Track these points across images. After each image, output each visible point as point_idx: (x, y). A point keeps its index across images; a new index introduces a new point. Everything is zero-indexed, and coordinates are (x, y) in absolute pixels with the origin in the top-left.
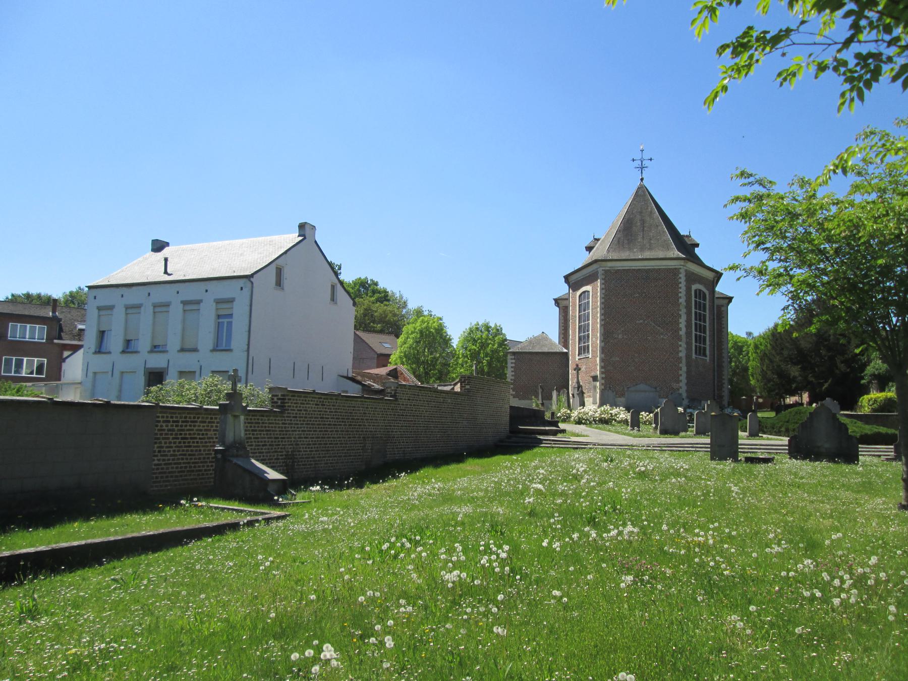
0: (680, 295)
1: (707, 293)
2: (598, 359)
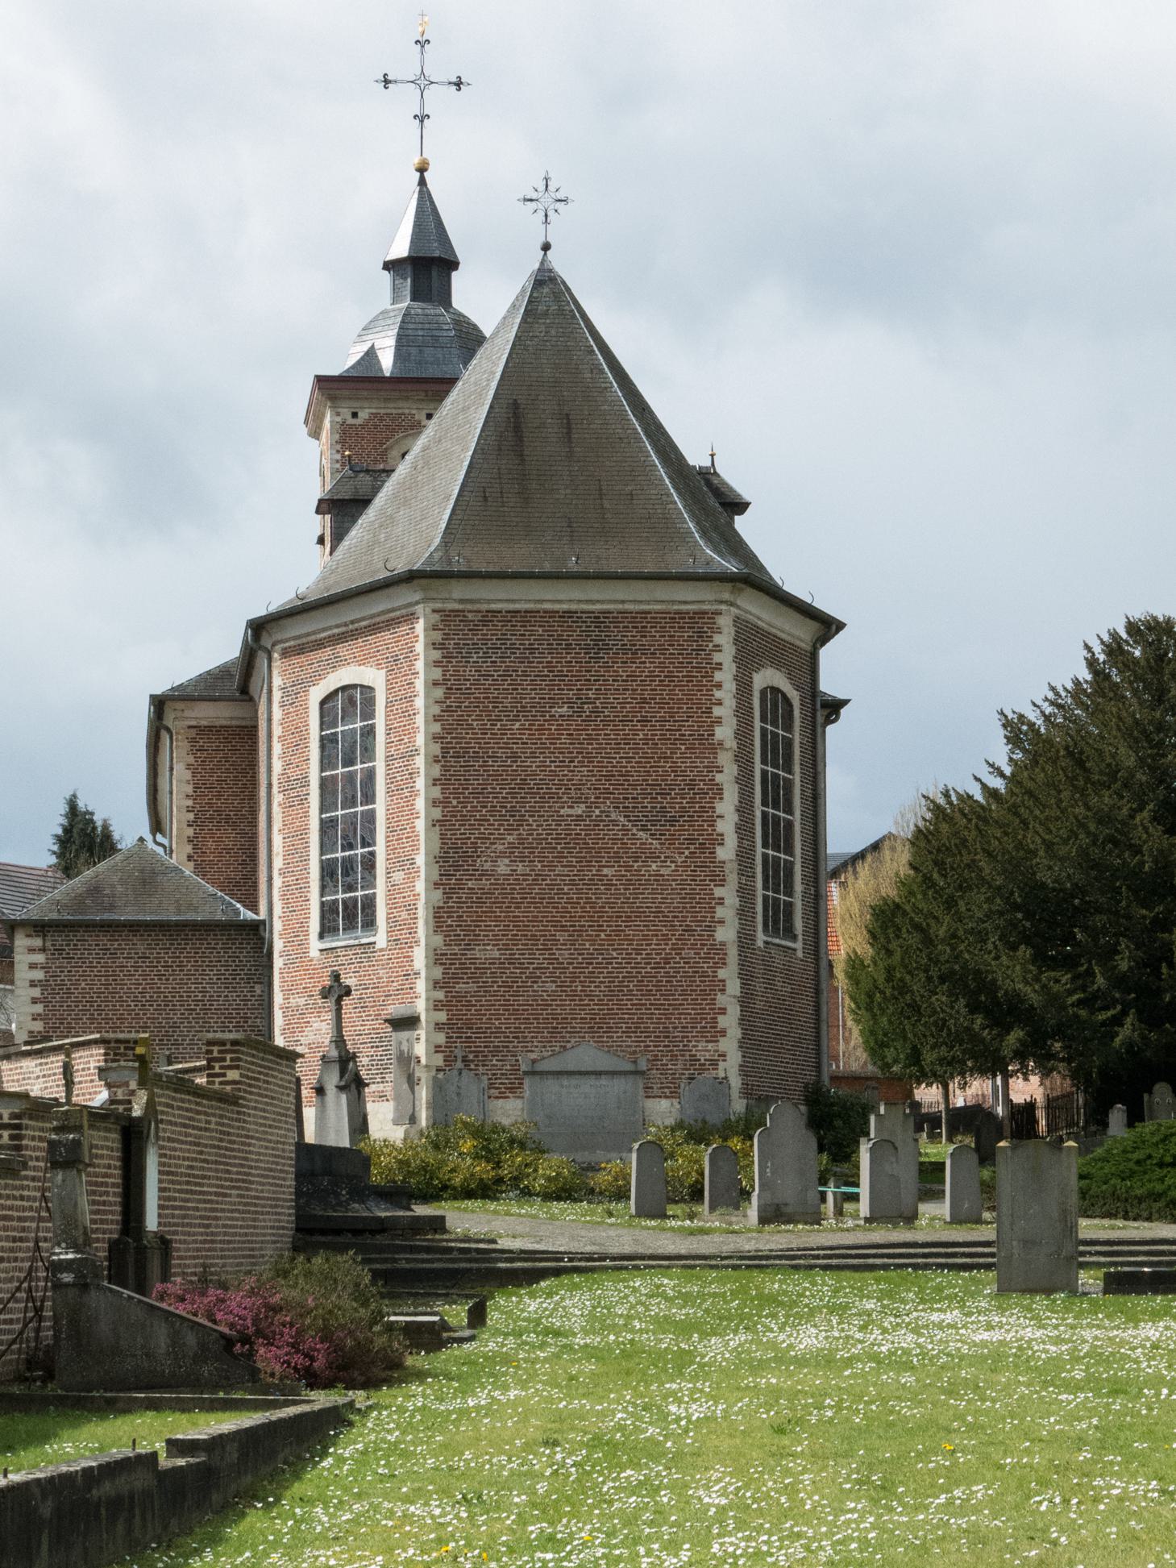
0: (717, 711)
1: (794, 696)
2: (419, 958)
